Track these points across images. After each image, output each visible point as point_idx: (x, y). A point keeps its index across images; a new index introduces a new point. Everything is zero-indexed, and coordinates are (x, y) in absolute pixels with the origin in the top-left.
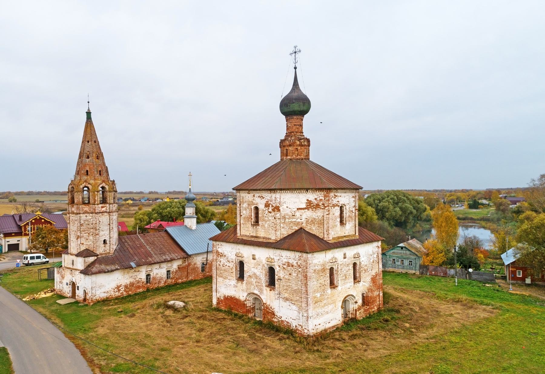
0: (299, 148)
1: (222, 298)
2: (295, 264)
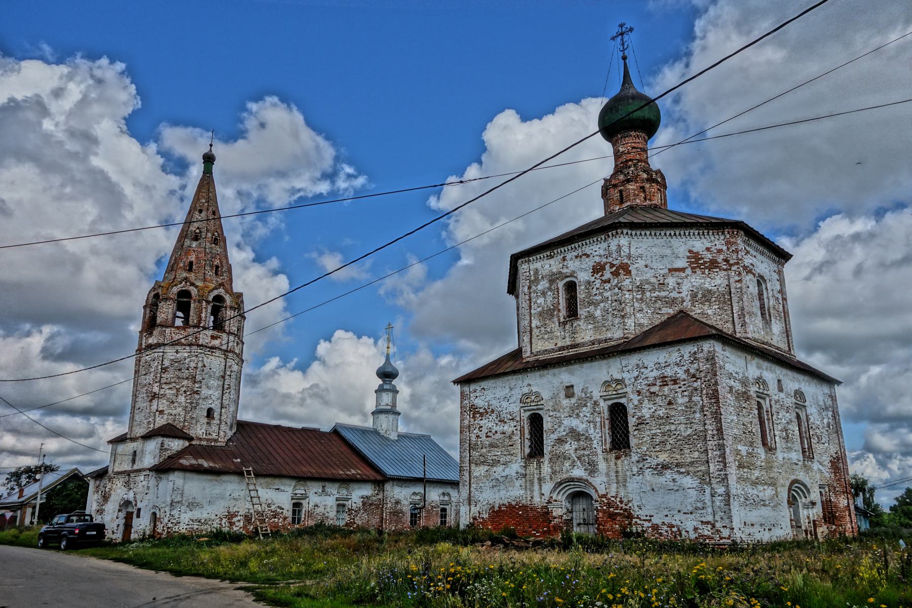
0: (647, 186)
1: (486, 516)
2: (681, 375)
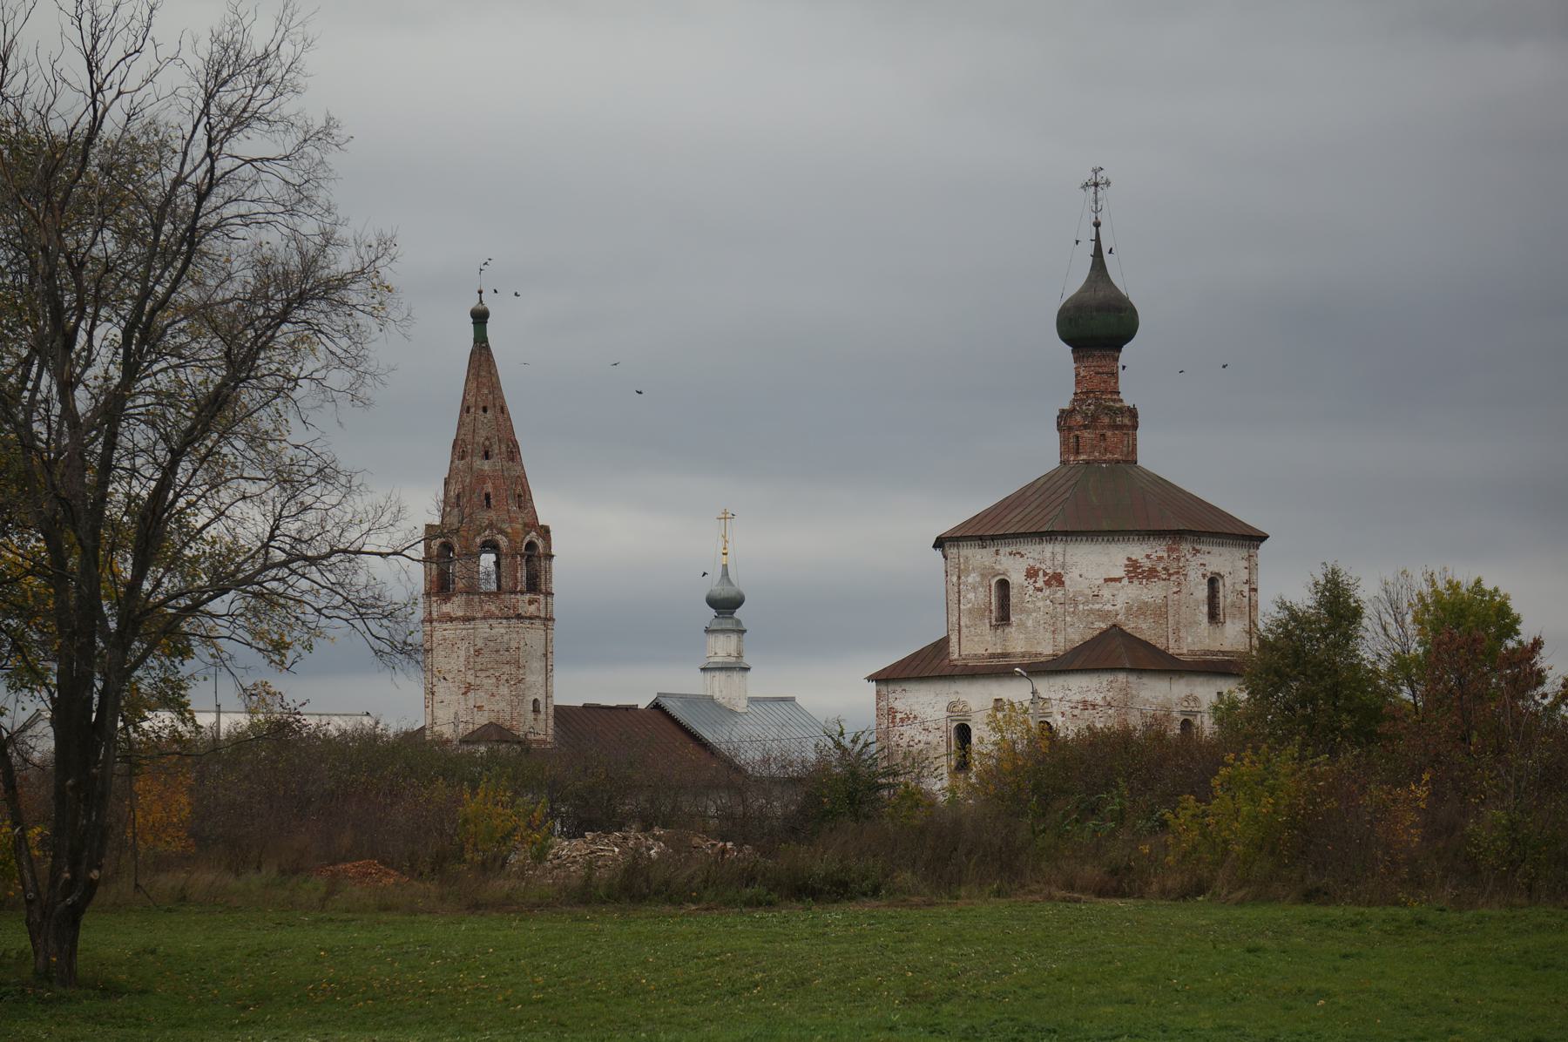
0: (1109, 434)
2: (1099, 701)
